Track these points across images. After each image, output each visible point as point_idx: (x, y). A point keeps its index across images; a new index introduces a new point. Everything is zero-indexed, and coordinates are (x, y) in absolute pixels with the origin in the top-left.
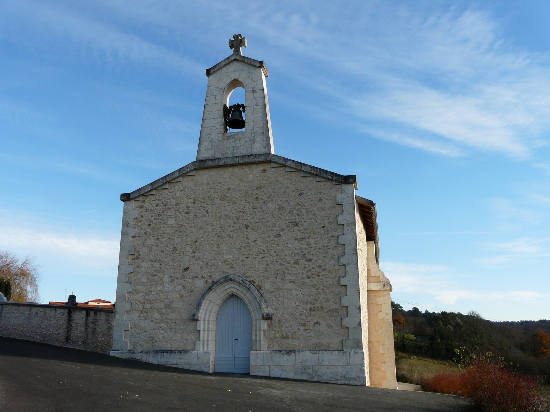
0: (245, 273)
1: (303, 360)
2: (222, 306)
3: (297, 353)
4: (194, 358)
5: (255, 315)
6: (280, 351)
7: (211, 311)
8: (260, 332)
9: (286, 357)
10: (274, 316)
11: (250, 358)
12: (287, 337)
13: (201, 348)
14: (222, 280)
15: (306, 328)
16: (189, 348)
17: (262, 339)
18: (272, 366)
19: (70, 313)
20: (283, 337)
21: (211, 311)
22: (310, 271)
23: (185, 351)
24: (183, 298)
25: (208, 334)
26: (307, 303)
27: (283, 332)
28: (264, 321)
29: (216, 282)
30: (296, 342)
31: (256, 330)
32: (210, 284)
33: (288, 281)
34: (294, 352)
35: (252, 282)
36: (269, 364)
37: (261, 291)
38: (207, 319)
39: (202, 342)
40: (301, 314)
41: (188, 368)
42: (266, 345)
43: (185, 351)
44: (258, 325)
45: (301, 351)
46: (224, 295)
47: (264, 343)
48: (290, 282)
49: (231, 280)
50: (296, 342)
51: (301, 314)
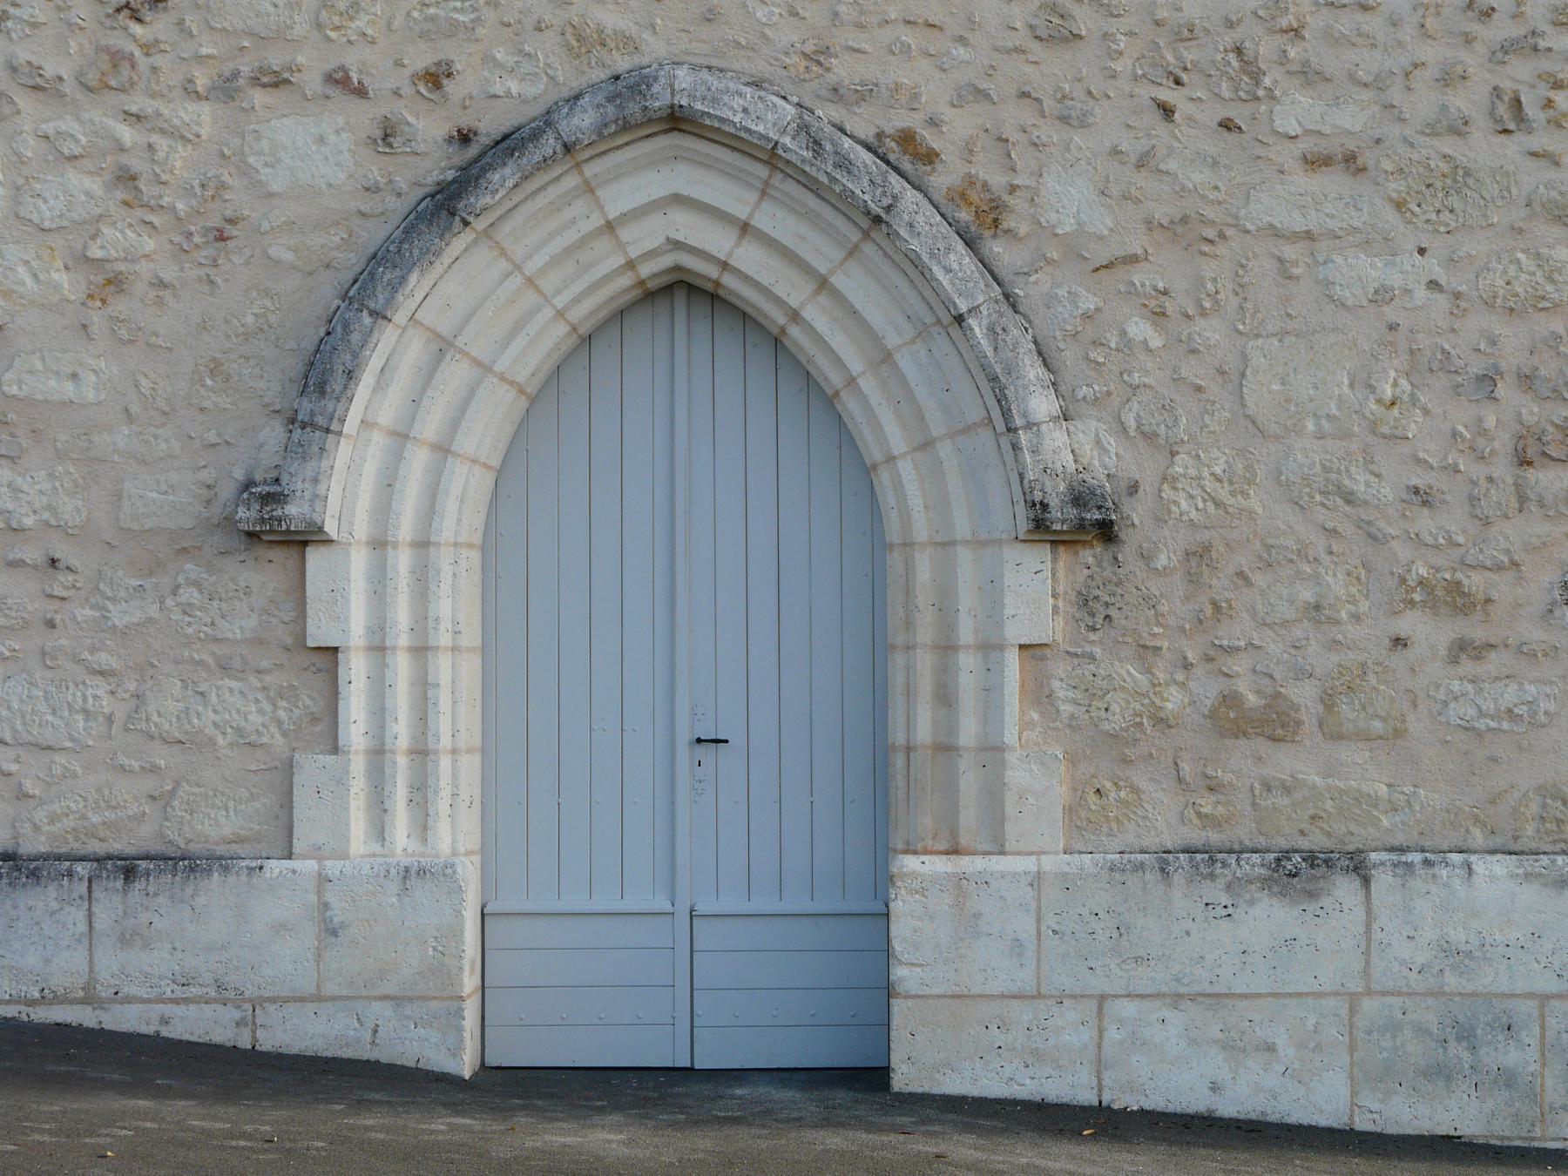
0: (818, 57)
1: (1447, 949)
2: (545, 395)
3: (1383, 880)
4: (281, 928)
5: (938, 497)
6: (1206, 857)
7: (443, 450)
8: (992, 670)
9: (1269, 916)
10: (1137, 513)
11: (900, 929)
12: (1275, 723)
13: (351, 830)
14: (582, 121)
15: (1478, 633)
16: (213, 826)
17: (1011, 735)
18: (1128, 1008)
19: (477, 363)
20: (1229, 720)
21: (443, 450)
22: (1529, 45)
23: (185, 864)
24: (120, 306)
25: (423, 688)
26: (1488, 381)
27: (1239, 665)
28: (1038, 558)
29: (509, 144)
30: (1364, 772)
31: (947, 648)
32: (430, 159)
33: (1287, 155)
34: (1359, 867)
35: (907, 153)
36: (1098, 984)
37: (996, 248)
38: (405, 530)
39: (358, 765)
40: (1422, 497)
41: (222, 1034)
42: (1059, 794)
43: (185, 864)
44: (967, 600)
45: (1420, 854)
46: (594, 282)
47: (1037, 782)
48: (1316, 162)
49: (677, 121)
50: (1364, 772)
51: (1422, 497)
